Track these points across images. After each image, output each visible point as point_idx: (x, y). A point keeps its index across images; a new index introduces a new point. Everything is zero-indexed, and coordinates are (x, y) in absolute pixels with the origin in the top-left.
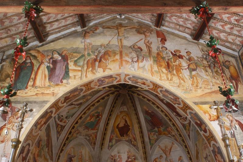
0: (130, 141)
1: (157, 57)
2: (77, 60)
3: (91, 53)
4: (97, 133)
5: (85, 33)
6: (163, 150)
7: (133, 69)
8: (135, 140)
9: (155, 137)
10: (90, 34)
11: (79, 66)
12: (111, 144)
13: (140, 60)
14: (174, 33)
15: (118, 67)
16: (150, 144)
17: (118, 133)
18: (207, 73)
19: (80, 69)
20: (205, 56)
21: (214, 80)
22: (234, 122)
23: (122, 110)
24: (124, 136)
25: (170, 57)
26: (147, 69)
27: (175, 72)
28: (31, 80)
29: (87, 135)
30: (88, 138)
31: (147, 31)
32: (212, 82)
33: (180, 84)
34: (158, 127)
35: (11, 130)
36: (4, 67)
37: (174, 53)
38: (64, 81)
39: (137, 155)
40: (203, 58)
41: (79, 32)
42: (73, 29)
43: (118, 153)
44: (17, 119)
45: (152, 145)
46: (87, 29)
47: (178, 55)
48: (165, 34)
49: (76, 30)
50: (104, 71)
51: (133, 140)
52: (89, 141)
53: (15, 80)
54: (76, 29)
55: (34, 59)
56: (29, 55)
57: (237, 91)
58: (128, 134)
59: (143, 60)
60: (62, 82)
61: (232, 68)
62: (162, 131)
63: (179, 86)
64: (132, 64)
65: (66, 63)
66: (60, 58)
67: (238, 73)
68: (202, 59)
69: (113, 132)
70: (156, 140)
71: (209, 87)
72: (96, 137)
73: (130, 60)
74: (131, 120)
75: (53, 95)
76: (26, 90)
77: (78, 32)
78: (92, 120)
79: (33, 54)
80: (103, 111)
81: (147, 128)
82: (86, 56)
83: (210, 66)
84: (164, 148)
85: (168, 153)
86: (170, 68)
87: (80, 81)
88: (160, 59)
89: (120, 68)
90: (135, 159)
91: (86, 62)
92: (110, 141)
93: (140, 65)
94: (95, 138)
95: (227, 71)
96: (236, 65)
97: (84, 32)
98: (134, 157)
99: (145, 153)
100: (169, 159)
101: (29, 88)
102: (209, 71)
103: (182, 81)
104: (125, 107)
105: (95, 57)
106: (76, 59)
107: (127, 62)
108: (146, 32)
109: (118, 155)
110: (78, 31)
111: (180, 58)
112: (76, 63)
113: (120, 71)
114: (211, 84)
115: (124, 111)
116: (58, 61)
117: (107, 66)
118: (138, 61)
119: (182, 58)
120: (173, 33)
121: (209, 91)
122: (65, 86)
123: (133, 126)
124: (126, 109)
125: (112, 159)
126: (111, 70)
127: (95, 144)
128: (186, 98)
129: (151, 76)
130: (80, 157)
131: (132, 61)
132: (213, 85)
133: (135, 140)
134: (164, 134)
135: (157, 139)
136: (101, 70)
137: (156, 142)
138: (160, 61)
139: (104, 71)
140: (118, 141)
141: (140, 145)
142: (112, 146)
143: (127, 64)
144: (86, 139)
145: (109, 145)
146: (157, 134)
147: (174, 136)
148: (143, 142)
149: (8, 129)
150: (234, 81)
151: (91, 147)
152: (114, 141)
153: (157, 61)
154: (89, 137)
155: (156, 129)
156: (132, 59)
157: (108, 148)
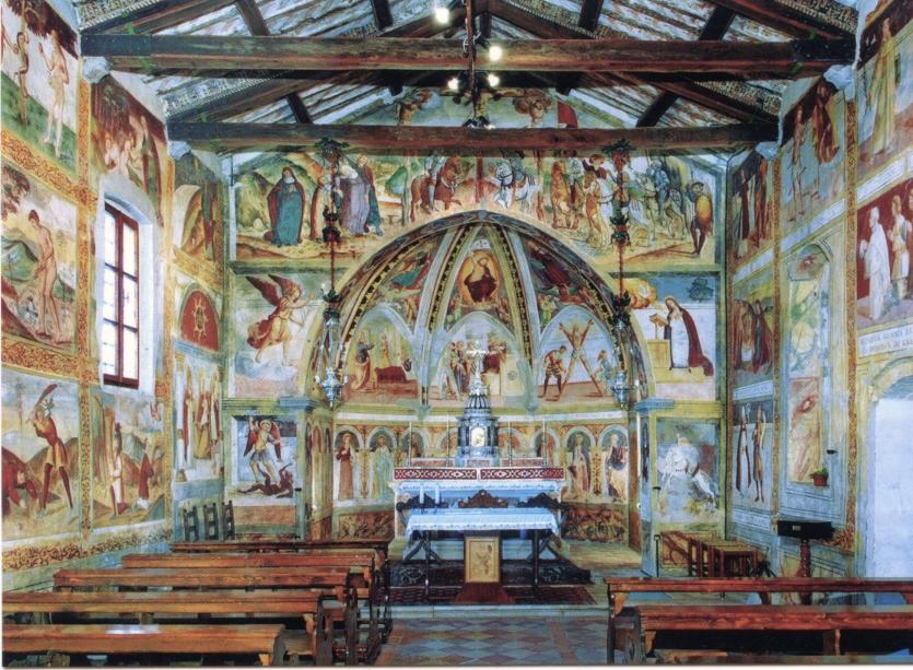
0: (495, 312)
1: (552, 175)
2: (390, 180)
3: (418, 164)
4: (419, 295)
5: (402, 111)
6: (568, 336)
7: (502, 203)
8: (507, 311)
9: (553, 306)
10: (413, 112)
11: (397, 195)
12: (450, 318)
13: (517, 182)
14: (598, 110)
15: (473, 199)
16: (541, 320)
17: (468, 294)
18: (649, 212)
19: (398, 201)
20: (653, 172)
21: (658, 229)
22: (677, 311)
23: (479, 248)
24: (480, 301)
25: (579, 175)
26: (530, 203)
27: (584, 210)
28: (305, 225)
29: (396, 300)
30: (399, 307)
31: (538, 105)
32: (653, 231)
33: (591, 235)
34: (558, 286)
35: (289, 321)
36: (242, 194)
37: (589, 164)
38: (372, 228)
39: (509, 343)
40: (647, 175)
41: (389, 105)
42: (374, 97)
43: (468, 337)
44: (295, 301)
45: (544, 322)
46: (405, 97)
47: (596, 168)
48: (577, 111)
49: (381, 100)
50: (446, 207)
51: (502, 310)
52: (401, 312)
53: (274, 224)
54: (380, 97)
55: (301, 174)
56: (288, 165)
57: (698, 251)
58: (492, 295)
59: (524, 181)
60: (367, 230)
61: (703, 202)
62: (568, 293)
63: (587, 241)
64: (500, 192)
65: (369, 186)
66: (355, 175)
67: (712, 213)
68: (644, 179)
69: (455, 291)
70: (555, 313)
71: (646, 244)
72: (417, 305)
73: (498, 183)
74: (497, 267)
75: (354, 257)
76: (300, 247)
77: (385, 106)
78: (409, 270)
79: (296, 163)
80: (435, 250)
81: (535, 285)
82: (409, 169)
83: (657, 196)
84: (571, 331)
85: (578, 343)
86: (576, 201)
87: (400, 227)
88: (558, 178)
89: (477, 201)
90: (504, 351)
91: (409, 186)
92: (449, 312)
93: (516, 194)
94: (414, 306)
95: (690, 205)
96: (713, 192)
97: (399, 108)
98: (502, 348)
99: (527, 339)
100: (577, 355)
101: (305, 241)
102: (654, 205)
103: (595, 230)
104: (484, 241)
105: (428, 174)
106: (388, 177)
107: (492, 185)
108: (535, 106)
109: (466, 341)
110: (385, 102)
111: (599, 176)
112: (389, 186)
113: (478, 207)
114: (651, 237)
115: (484, 250)
116: (353, 182)
117: (451, 196)
118: (512, 185)
119: (604, 177)
120: (593, 108)
121: (644, 251)
122: (374, 238)
123: (502, 280)
124: (487, 246)
125: (453, 350)
126: (460, 204)
127: (414, 318)
128: (597, 266)
129: (536, 219)
130: (384, 348)
131: (502, 184)
132: (654, 239)
133: (507, 311)
134: (574, 300)
135: (557, 311)
136: (439, 204)
137: (553, 315)
138: (556, 186)
139: (446, 207)
140: (465, 311)
141: (517, 321)
142: (453, 322)
143: (490, 191)
144: (395, 308)
145: (446, 320)
146: (557, 299)
147: (593, 307)
148: (524, 316)
149: (282, 319)
150: (698, 231)
151: (406, 326)
152: (457, 313)
153: (551, 184)
154: (401, 304)
155: (556, 289)
156: (502, 178)
157: (445, 328)
